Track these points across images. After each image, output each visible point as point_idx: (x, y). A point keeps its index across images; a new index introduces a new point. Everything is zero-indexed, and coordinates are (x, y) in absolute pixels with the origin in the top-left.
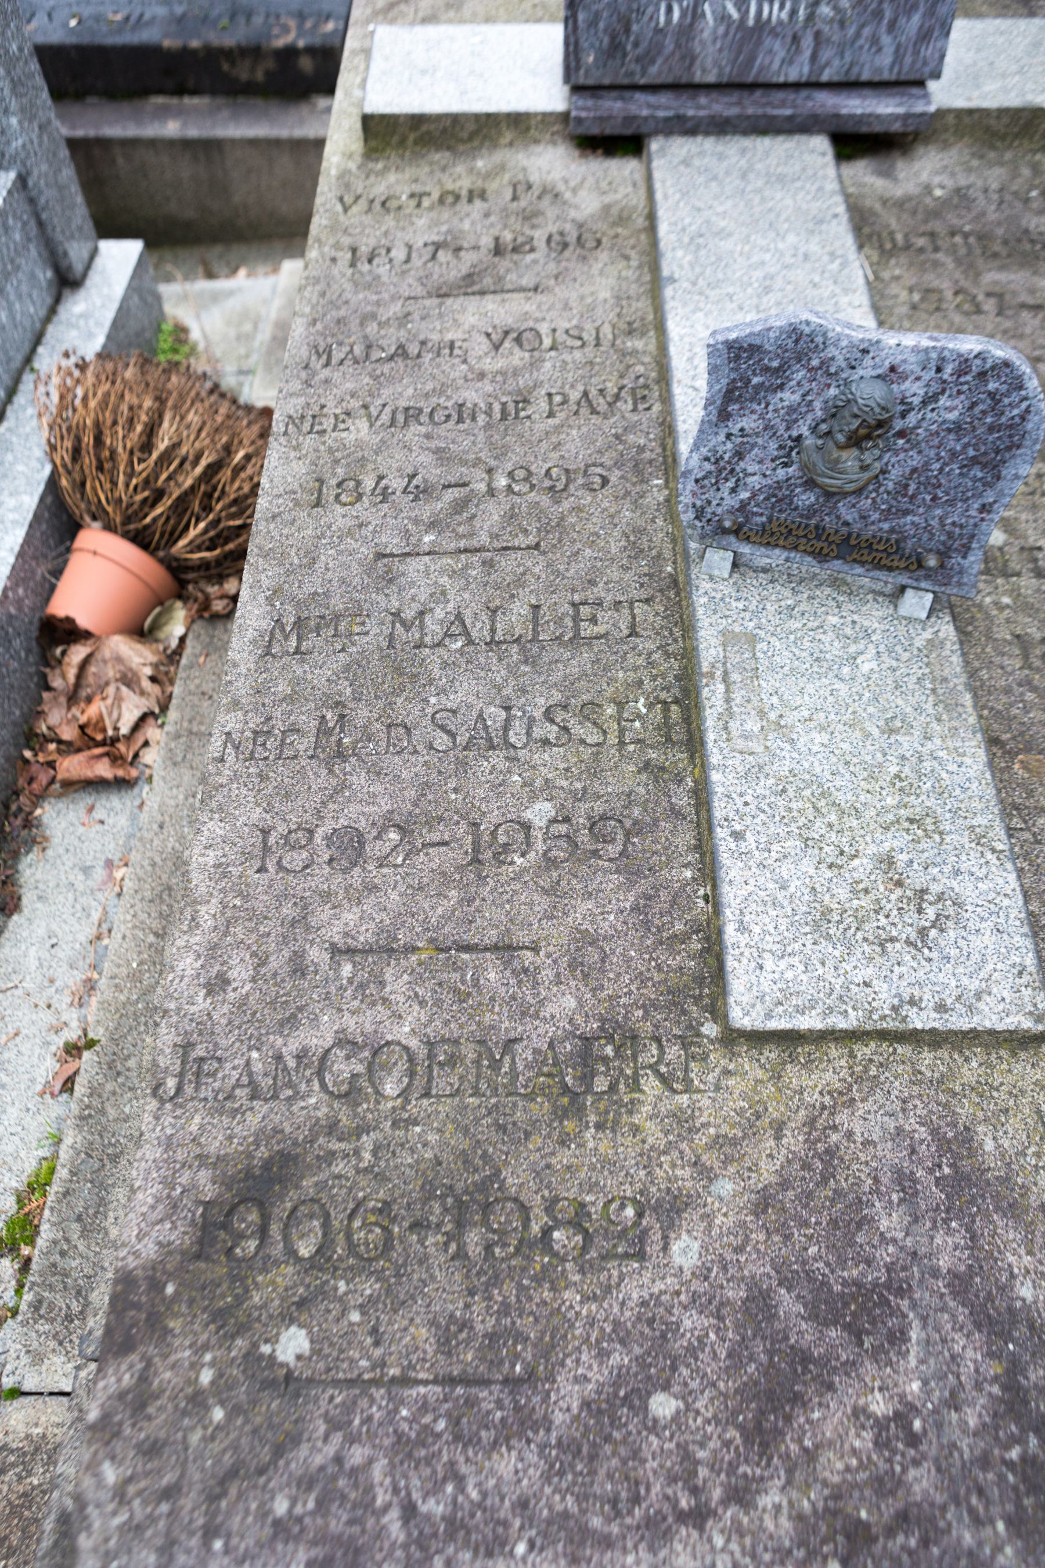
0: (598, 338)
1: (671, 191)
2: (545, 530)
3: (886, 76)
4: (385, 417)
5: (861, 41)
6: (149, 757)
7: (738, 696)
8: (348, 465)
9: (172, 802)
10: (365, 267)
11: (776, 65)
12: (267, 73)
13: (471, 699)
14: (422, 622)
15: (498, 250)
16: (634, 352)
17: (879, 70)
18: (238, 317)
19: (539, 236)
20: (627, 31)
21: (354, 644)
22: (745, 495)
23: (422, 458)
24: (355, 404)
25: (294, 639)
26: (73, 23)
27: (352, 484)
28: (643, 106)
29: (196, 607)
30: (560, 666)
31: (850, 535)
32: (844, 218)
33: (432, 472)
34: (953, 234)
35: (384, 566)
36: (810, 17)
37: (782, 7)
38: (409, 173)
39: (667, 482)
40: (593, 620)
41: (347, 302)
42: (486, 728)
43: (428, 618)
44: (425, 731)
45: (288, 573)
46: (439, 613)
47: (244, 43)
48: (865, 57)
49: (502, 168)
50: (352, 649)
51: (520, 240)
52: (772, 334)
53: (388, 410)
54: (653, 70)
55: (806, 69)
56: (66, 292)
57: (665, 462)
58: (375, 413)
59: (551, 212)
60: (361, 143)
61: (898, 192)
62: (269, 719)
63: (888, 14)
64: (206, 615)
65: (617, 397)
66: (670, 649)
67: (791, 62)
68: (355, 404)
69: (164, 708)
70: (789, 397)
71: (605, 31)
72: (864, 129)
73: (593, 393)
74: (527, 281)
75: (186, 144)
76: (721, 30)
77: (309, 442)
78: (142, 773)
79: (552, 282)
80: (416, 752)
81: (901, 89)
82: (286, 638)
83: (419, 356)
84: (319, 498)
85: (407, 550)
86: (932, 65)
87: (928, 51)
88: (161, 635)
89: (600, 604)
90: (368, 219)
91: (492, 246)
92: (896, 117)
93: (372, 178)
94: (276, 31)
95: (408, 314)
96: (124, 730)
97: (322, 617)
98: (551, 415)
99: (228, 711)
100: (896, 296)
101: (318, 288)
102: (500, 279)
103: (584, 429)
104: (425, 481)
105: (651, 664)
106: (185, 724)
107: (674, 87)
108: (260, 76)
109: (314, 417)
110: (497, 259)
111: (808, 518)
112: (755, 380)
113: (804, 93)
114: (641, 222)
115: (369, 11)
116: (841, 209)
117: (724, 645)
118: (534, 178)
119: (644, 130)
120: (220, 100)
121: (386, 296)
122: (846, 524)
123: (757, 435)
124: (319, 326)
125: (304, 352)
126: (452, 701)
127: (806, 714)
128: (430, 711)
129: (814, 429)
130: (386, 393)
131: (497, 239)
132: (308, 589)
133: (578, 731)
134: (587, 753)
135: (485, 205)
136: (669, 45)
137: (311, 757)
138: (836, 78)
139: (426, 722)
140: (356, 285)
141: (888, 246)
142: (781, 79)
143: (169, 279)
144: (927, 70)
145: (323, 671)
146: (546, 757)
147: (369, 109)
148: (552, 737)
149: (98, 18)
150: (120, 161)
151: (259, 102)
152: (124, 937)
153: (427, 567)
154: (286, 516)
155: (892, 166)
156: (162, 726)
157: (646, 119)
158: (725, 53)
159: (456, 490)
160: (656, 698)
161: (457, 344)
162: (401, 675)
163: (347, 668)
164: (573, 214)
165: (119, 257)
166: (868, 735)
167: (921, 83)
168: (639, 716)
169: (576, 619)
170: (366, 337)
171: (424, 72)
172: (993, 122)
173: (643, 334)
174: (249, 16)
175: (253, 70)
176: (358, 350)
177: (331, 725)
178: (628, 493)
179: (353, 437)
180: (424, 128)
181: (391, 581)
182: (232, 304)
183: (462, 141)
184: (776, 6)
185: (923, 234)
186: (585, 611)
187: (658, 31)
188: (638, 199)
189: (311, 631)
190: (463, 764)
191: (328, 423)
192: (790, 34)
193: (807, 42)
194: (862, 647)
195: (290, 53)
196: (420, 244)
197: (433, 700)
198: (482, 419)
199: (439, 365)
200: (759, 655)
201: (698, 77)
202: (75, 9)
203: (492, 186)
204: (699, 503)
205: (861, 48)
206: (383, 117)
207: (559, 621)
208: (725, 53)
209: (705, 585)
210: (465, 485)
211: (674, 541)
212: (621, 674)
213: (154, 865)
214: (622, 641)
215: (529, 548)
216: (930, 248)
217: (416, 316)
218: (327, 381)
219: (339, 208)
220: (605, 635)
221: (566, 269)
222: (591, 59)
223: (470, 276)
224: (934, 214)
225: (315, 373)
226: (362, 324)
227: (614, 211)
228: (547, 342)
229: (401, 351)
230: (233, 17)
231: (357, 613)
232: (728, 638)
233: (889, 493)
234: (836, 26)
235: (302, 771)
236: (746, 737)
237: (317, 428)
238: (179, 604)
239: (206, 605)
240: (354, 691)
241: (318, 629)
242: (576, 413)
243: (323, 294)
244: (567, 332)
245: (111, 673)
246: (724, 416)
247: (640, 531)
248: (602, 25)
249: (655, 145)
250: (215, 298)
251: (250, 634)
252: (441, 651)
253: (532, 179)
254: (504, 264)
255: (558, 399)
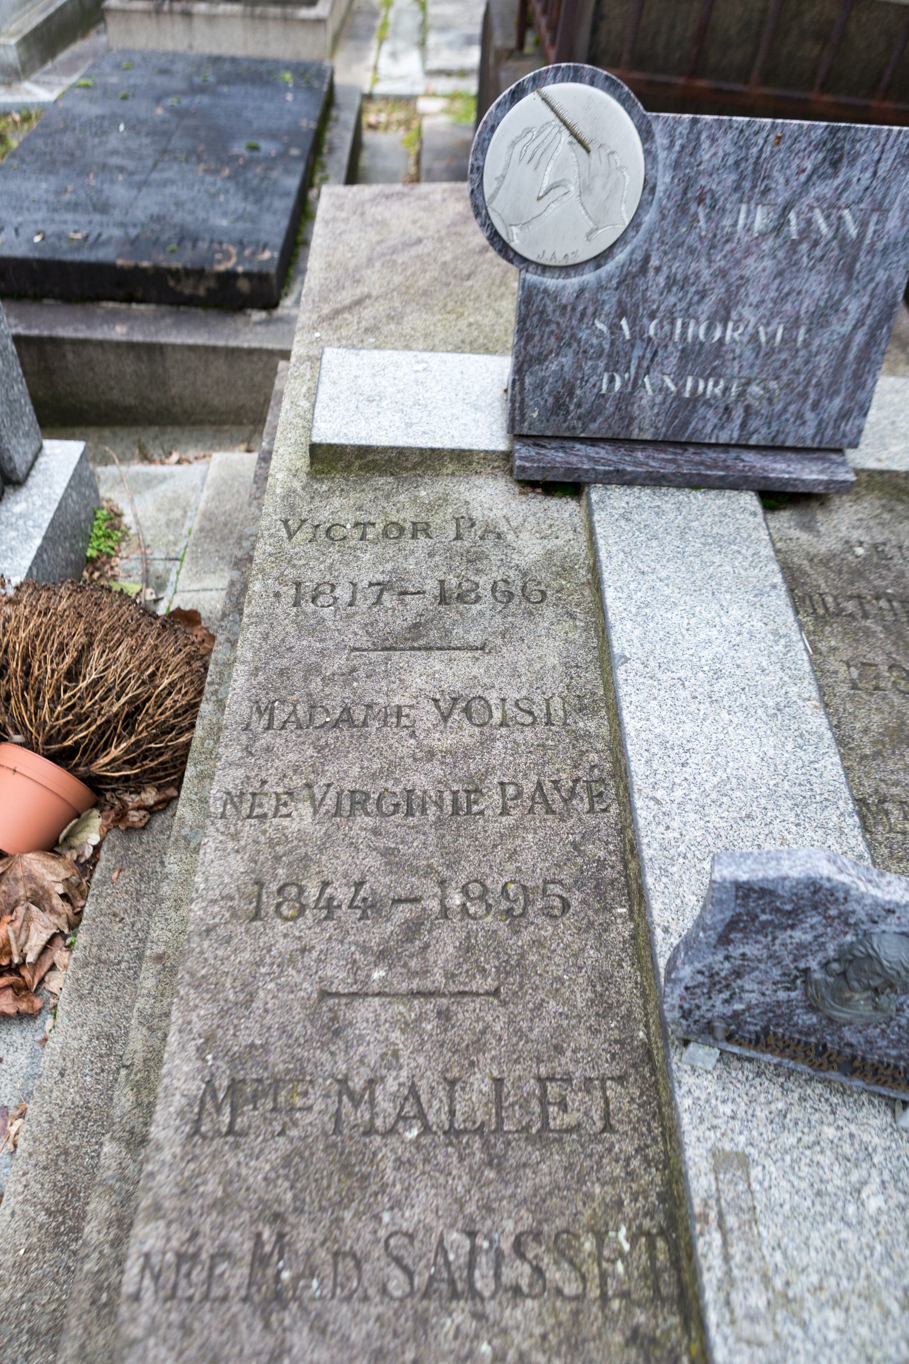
0: (548, 714)
1: (614, 549)
2: (504, 971)
3: (809, 443)
4: (330, 802)
5: (788, 415)
6: (55, 983)
7: (737, 1250)
8: (290, 865)
9: (75, 1044)
10: (310, 608)
11: (708, 429)
12: (208, 290)
13: (430, 1218)
14: (372, 1094)
15: (443, 598)
16: (587, 735)
17: (803, 439)
18: (169, 502)
19: (484, 581)
20: (571, 394)
21: (295, 1124)
22: (738, 1007)
23: (369, 862)
24: (298, 782)
25: (227, 1110)
26: (37, 239)
27: (294, 890)
28: (582, 458)
29: (112, 815)
30: (529, 1172)
31: (854, 1058)
32: (782, 589)
33: (381, 883)
34: (878, 598)
35: (328, 1018)
36: (742, 394)
37: (716, 384)
38: (354, 498)
39: (631, 911)
40: (563, 1106)
41: (289, 649)
42: (448, 1264)
43: (379, 1089)
44: (377, 1263)
45: (224, 1013)
46: (392, 1085)
47: (189, 266)
48: (790, 428)
49: (445, 499)
50: (294, 1133)
51: (466, 586)
52: (787, 883)
53: (332, 793)
54: (593, 426)
55: (736, 434)
56: (9, 490)
57: (627, 885)
58: (319, 796)
59: (495, 556)
60: (308, 461)
61: (822, 548)
62: (195, 1235)
63: (812, 396)
64: (122, 827)
65: (572, 792)
66: (650, 1152)
67: (722, 428)
68: (298, 782)
69: (74, 926)
70: (798, 935)
71: (550, 394)
72: (790, 489)
73: (548, 785)
74: (474, 637)
75: (132, 346)
76: (659, 399)
77: (248, 829)
78: (47, 1002)
79: (499, 641)
80: (366, 1298)
81: (821, 455)
82: (219, 1109)
83: (365, 724)
84: (258, 908)
85: (354, 988)
86: (851, 437)
87: (847, 427)
88: (76, 842)
89: (569, 1080)
90: (312, 549)
91: (437, 593)
92: (820, 482)
93: (317, 502)
94: (218, 256)
95: (354, 670)
96: (30, 958)
97: (259, 1081)
98: (505, 812)
99: (148, 1220)
100: (836, 672)
101: (261, 629)
102: (447, 633)
103: (541, 834)
104: (373, 892)
105: (631, 1175)
106: (94, 950)
107: (614, 441)
108: (202, 292)
109: (254, 795)
110: (441, 608)
111: (807, 1034)
112: (763, 917)
113: (733, 453)
114: (583, 575)
115: (315, 317)
116: (778, 579)
117: (716, 1172)
118: (476, 514)
119: (584, 479)
120: (164, 308)
121: (330, 644)
122: (850, 1045)
123: (760, 961)
124: (261, 678)
125: (245, 709)
126: (409, 1218)
127: (815, 1279)
128: (382, 1233)
129: (825, 966)
130: (331, 769)
131: (442, 582)
132: (245, 1039)
133: (554, 1275)
134: (565, 1310)
135: (430, 542)
136: (610, 407)
137: (245, 1300)
138: (763, 443)
139: (378, 1251)
140: (300, 628)
141: (821, 611)
142: (713, 441)
143: (106, 461)
144: (846, 441)
145: (258, 1167)
146: (518, 1314)
147: (316, 439)
148: (524, 1283)
149: (60, 236)
150: (70, 356)
151: (200, 311)
152: (13, 1214)
153: (377, 1016)
154: (221, 931)
155: (813, 519)
156: (69, 947)
157: (587, 471)
158: (662, 417)
159: (408, 906)
160: (640, 1227)
161: (406, 711)
162: (350, 1175)
163: (287, 1161)
164: (516, 559)
165: (61, 456)
166: (887, 1314)
167: (839, 451)
168: (621, 1255)
169: (544, 1102)
170: (309, 695)
171: (370, 401)
172: (901, 481)
173: (595, 713)
174: (195, 241)
175: (196, 287)
176: (301, 710)
177: (268, 1248)
178: (591, 924)
179: (295, 826)
180: (370, 457)
181: (337, 1033)
182: (163, 489)
183: (406, 469)
184: (711, 383)
185: (851, 597)
186: (553, 1089)
187: (599, 396)
188: (579, 547)
189: (246, 1102)
190: (422, 1321)
191: (269, 805)
192: (723, 406)
193: (738, 414)
194: (864, 1173)
195: (231, 276)
196: (365, 583)
197: (386, 1217)
198: (432, 810)
199: (386, 738)
200: (755, 1186)
201: (635, 435)
202: (40, 227)
203: (436, 520)
204: (686, 1006)
205: (787, 420)
206: (330, 446)
207: (524, 1105)
208: (662, 417)
209: (688, 1080)
210: (417, 900)
211: (644, 995)
212: (597, 1190)
213: (51, 1122)
214: (596, 1138)
215: (487, 993)
216: (860, 614)
217: (361, 673)
218: (268, 749)
219: (283, 533)
220: (576, 1128)
221: (513, 626)
222: (535, 415)
223: (416, 626)
224: (858, 574)
225: (255, 738)
226: (305, 679)
227: (556, 559)
228: (497, 715)
229: (346, 718)
230: (180, 242)
231: (299, 1076)
232: (721, 1161)
233: (900, 1027)
234: (765, 402)
235: (232, 1323)
236: (752, 1318)
237: (257, 811)
238: (96, 812)
239: (122, 815)
240: (295, 1198)
241: (255, 1098)
242: (531, 810)
243: (266, 637)
244: (517, 704)
245: (22, 891)
246: (724, 940)
247: (606, 978)
248: (547, 388)
249: (595, 494)
250: (149, 482)
251: (178, 1101)
252: (393, 1140)
253: (475, 514)
254: (451, 614)
255: (511, 790)
